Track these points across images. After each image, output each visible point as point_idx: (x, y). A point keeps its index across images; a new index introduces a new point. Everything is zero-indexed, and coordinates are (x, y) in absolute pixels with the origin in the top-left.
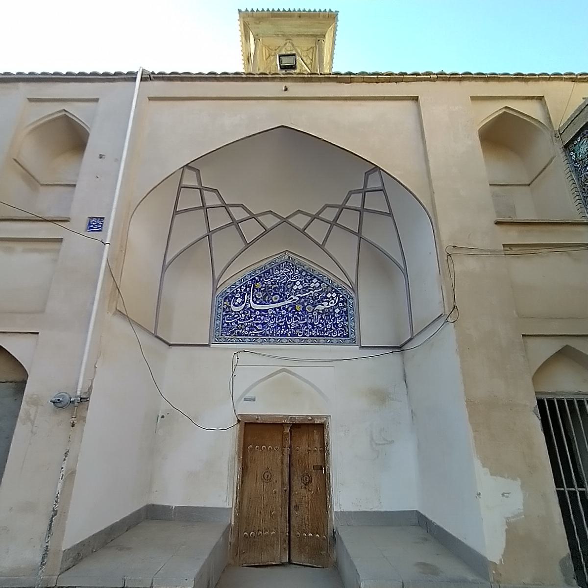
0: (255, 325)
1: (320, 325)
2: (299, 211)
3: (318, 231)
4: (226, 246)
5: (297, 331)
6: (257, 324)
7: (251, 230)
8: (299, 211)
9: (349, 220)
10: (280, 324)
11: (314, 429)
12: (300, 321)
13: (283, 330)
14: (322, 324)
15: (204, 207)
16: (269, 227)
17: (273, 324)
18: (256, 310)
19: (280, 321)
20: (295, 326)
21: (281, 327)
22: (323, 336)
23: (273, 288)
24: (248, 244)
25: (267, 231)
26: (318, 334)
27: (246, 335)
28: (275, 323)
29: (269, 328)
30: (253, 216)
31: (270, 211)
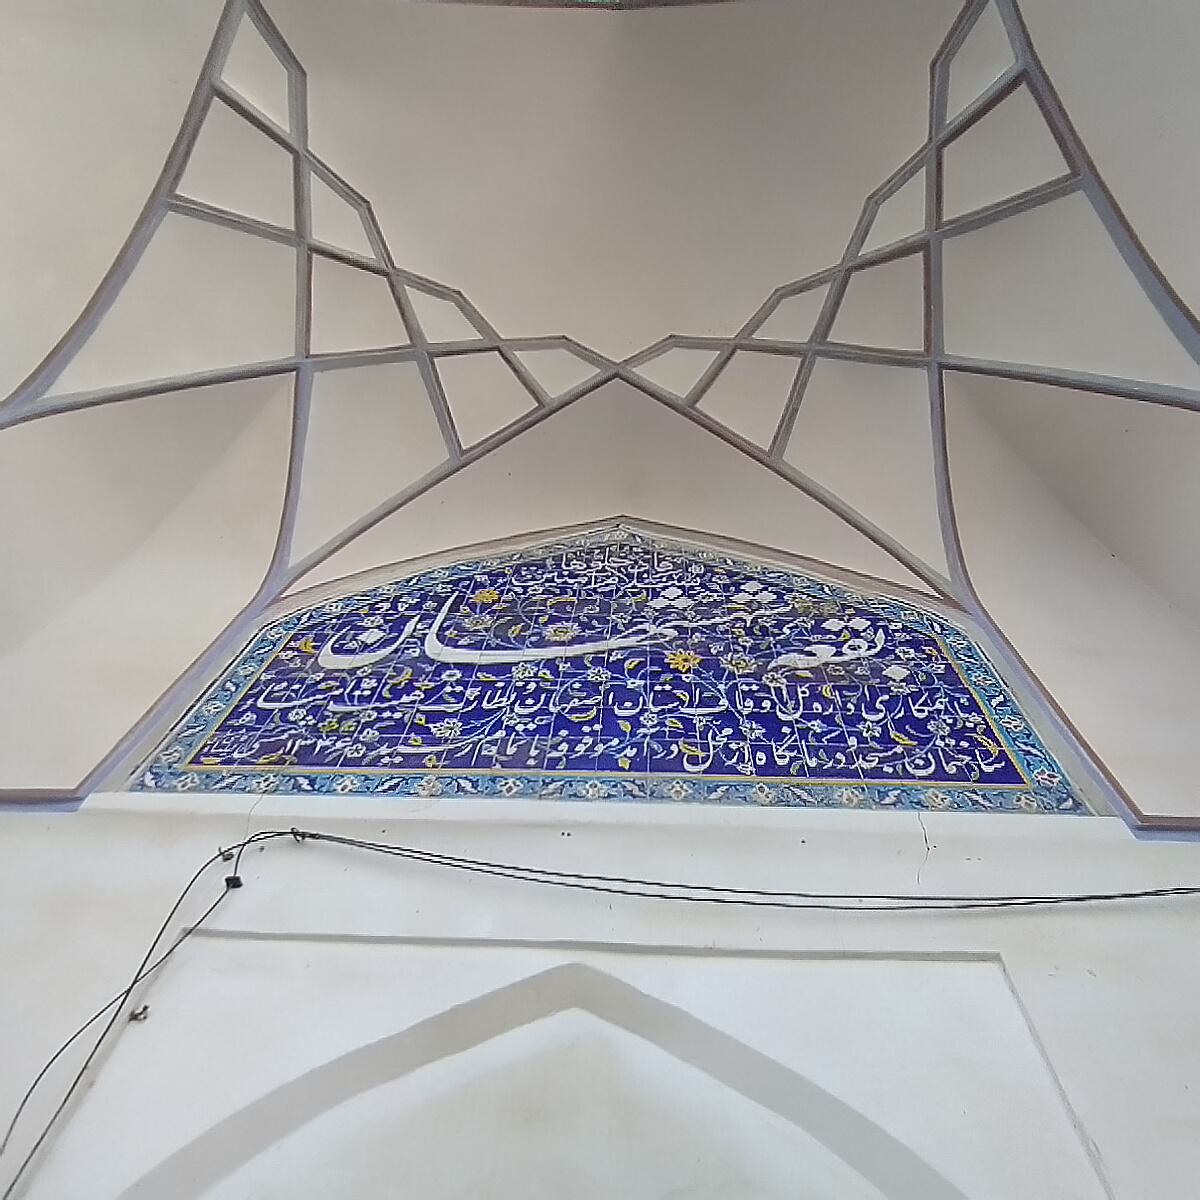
0: (421, 720)
1: (817, 726)
2: (675, 341)
3: (748, 403)
4: (363, 449)
5: (674, 748)
6: (433, 717)
7: (483, 398)
8: (675, 341)
9: (883, 316)
10: (573, 718)
11: (226, 880)
12: (690, 705)
13: (589, 740)
14: (828, 720)
15: (298, 236)
16: (554, 392)
17: (533, 716)
18: (446, 666)
19: (575, 703)
20: (662, 724)
21: (576, 729)
22: (855, 774)
23: (548, 604)
24: (463, 452)
25: (545, 411)
26: (813, 763)
27: (347, 763)
28: (544, 711)
29: (500, 734)
30: (493, 345)
31: (564, 337)
